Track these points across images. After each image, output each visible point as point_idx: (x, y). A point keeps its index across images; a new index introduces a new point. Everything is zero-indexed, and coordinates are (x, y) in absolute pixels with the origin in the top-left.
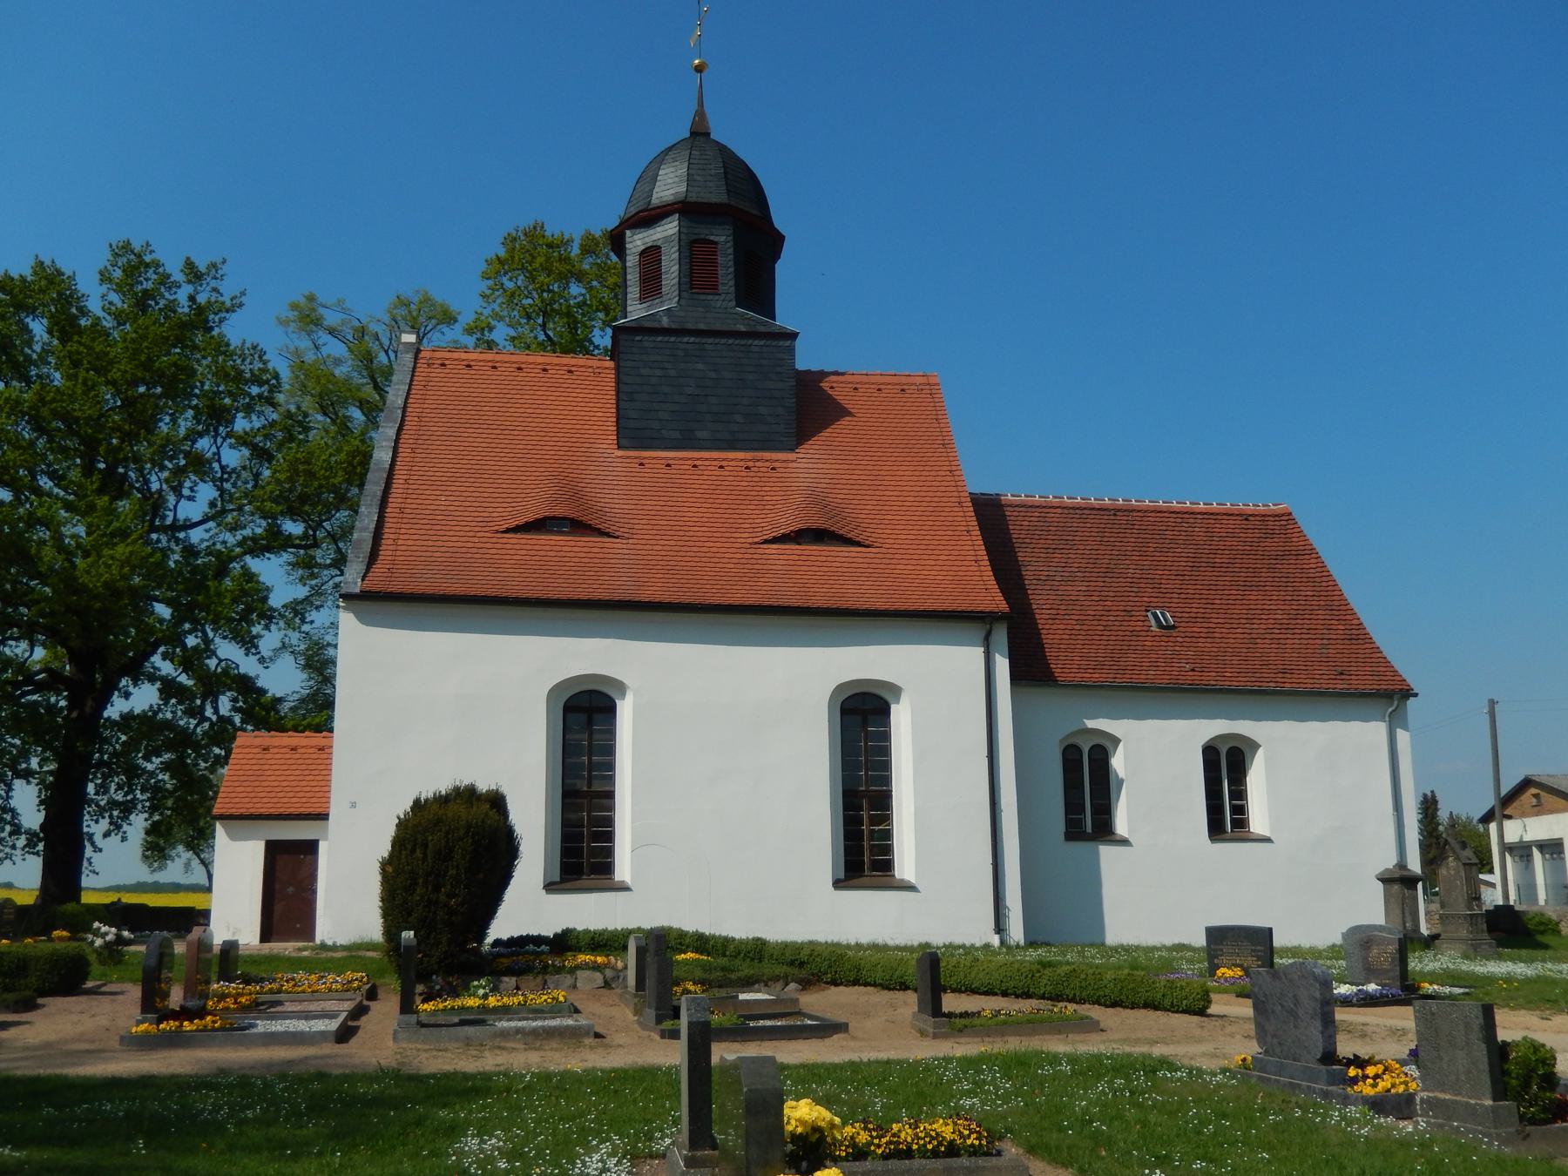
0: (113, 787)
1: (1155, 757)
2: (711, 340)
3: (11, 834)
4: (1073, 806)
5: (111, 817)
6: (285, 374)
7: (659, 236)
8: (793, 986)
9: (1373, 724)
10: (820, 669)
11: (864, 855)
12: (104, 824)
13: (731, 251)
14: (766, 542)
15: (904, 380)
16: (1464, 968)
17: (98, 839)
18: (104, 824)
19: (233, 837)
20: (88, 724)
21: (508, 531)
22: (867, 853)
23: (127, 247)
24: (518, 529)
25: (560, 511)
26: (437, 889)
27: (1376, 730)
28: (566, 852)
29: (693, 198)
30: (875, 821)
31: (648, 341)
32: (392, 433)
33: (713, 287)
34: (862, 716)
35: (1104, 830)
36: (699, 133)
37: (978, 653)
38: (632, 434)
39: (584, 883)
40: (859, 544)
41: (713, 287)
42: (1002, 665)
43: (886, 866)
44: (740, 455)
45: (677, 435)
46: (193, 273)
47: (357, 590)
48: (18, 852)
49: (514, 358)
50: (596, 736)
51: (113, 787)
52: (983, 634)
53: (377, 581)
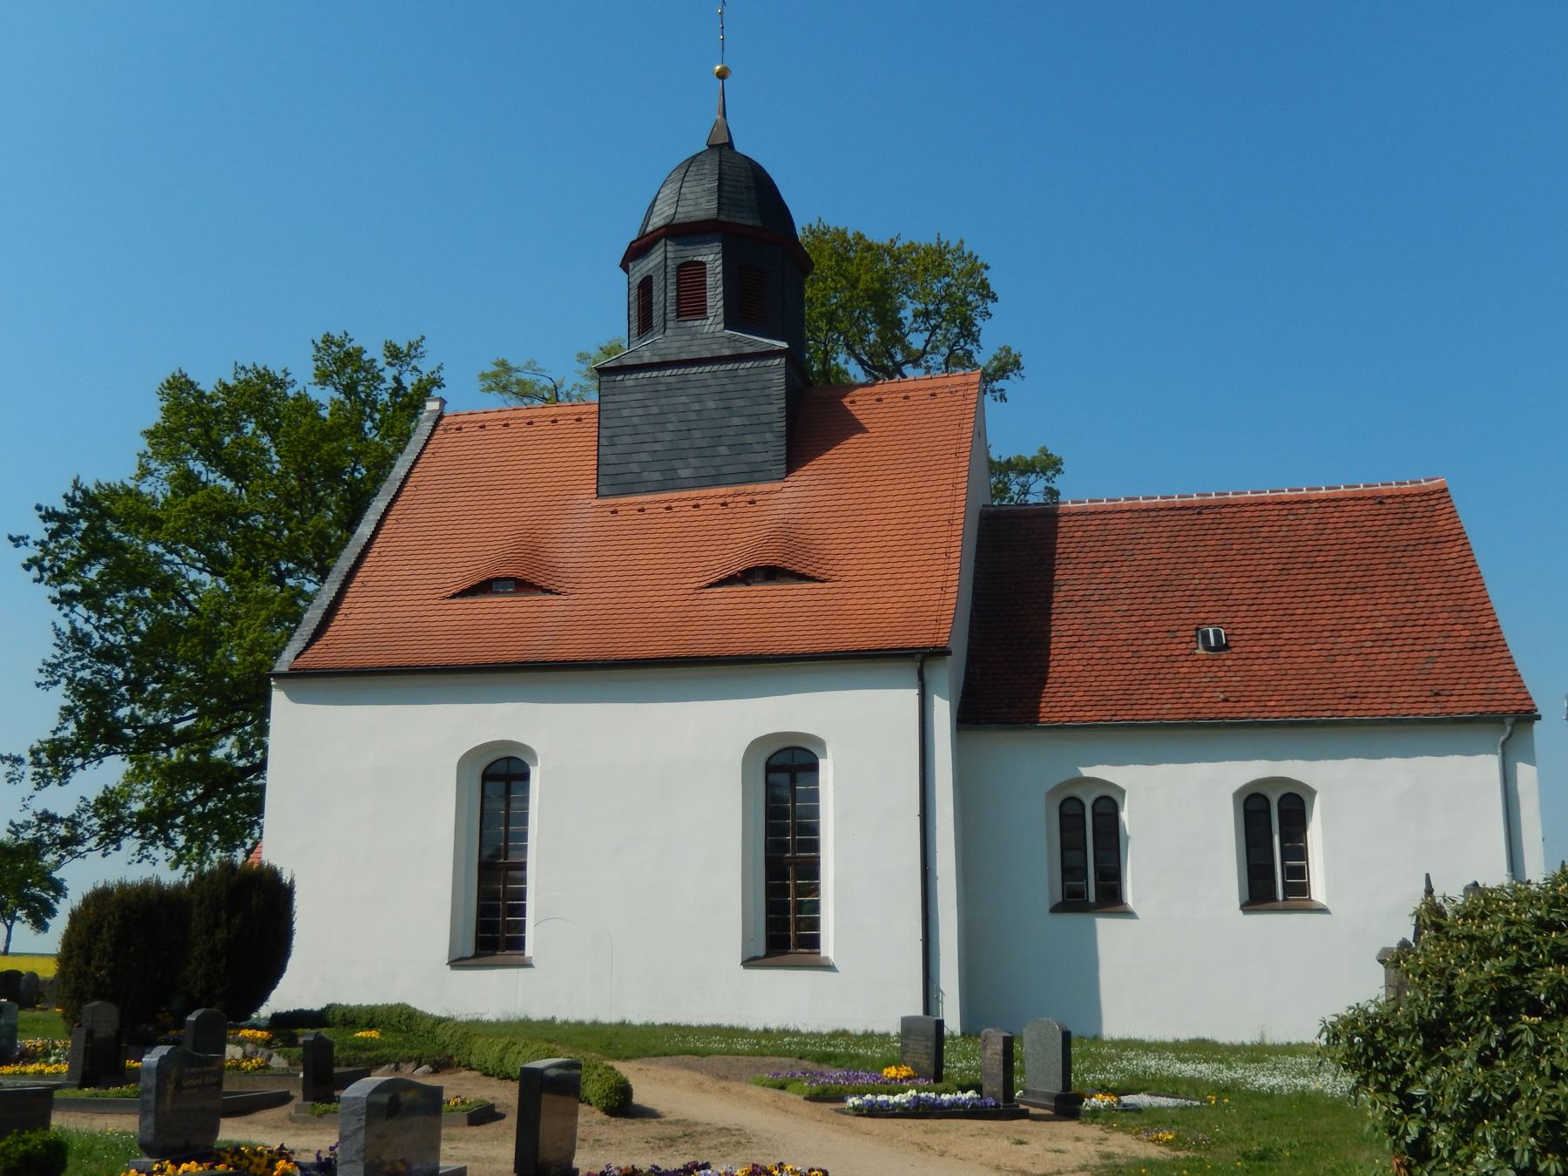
1: (1179, 813)
2: (694, 370)
4: (1071, 871)
8: (425, 1068)
9: (1482, 757)
10: (719, 730)
11: (785, 924)
13: (720, 269)
15: (482, 417)
16: (1203, 1067)
21: (454, 596)
22: (792, 927)
23: (328, 340)
26: (88, 964)
27: (1487, 766)
29: (680, 218)
30: (801, 891)
31: (630, 380)
33: (701, 312)
34: (786, 772)
35: (1111, 898)
36: (722, 148)
37: (909, 697)
38: (614, 480)
39: (500, 957)
41: (701, 312)
42: (942, 710)
43: (813, 943)
44: (722, 491)
45: (657, 476)
46: (394, 354)
49: (546, 411)
50: (513, 805)
52: (914, 677)
53: (320, 656)
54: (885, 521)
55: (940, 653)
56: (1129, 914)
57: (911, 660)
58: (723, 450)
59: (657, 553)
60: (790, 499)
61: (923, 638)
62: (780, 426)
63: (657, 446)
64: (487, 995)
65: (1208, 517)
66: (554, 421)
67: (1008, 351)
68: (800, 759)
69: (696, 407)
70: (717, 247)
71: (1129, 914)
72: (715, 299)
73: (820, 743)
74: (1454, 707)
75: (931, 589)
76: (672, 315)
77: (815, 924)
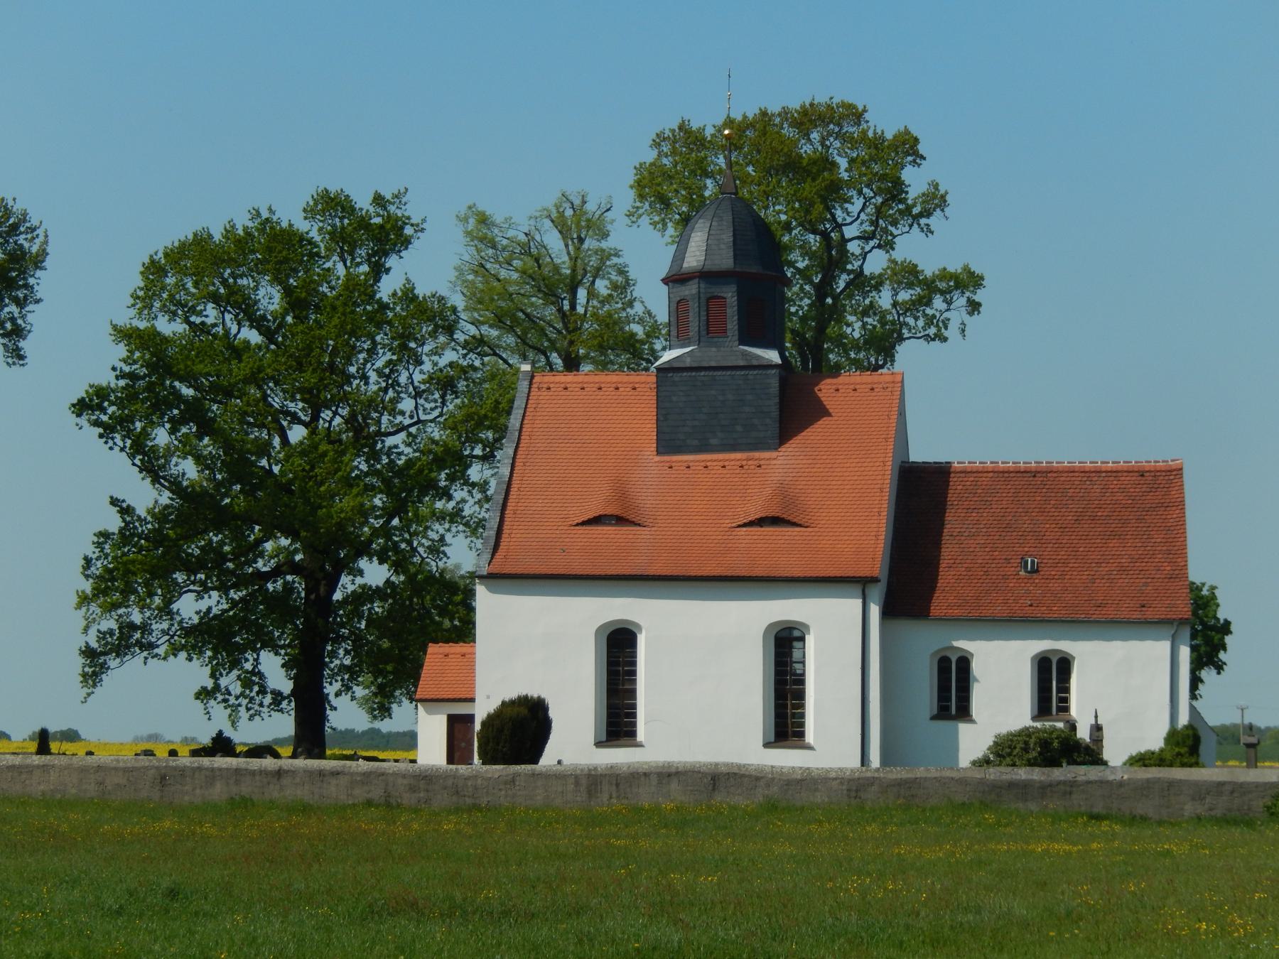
0: (341, 652)
3: (258, 693)
5: (342, 680)
6: (458, 301)
7: (687, 293)
10: (754, 616)
11: (786, 724)
12: (337, 686)
14: (739, 526)
17: (332, 697)
18: (337, 686)
19: (429, 712)
20: (321, 604)
21: (577, 525)
24: (584, 523)
25: (609, 511)
26: (498, 744)
28: (609, 724)
31: (677, 377)
32: (511, 452)
35: (964, 713)
38: (668, 443)
39: (622, 742)
40: (800, 526)
42: (875, 611)
43: (801, 735)
44: (738, 455)
45: (696, 442)
47: (485, 573)
48: (265, 710)
51: (341, 652)
54: (837, 482)
55: (874, 580)
56: (972, 721)
57: (859, 583)
58: (739, 428)
59: (720, 488)
60: (782, 463)
61: (864, 572)
62: (775, 414)
63: (696, 423)
64: (786, 759)
65: (1039, 479)
66: (617, 389)
67: (936, 186)
68: (796, 634)
69: (721, 398)
70: (733, 288)
71: (972, 721)
72: (732, 325)
73: (807, 627)
74: (1150, 614)
75: (868, 536)
76: (704, 333)
77: (802, 725)
